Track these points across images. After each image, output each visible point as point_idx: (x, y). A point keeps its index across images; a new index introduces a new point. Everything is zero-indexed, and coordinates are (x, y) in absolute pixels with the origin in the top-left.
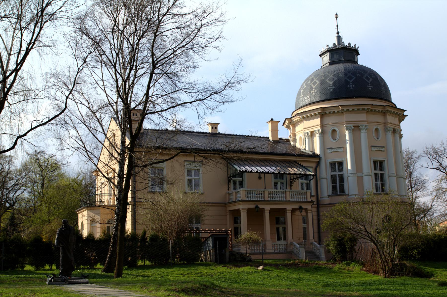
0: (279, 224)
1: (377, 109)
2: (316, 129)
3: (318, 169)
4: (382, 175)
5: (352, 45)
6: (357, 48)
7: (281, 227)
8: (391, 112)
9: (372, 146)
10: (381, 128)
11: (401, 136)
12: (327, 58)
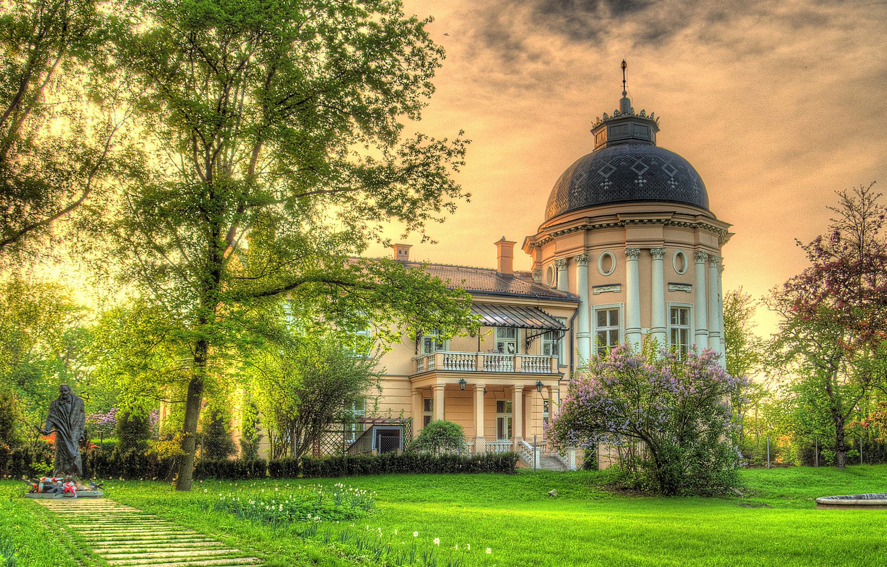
0: (502, 412)
1: (604, 223)
2: (577, 254)
3: (575, 321)
4: (684, 332)
5: (648, 114)
6: (655, 118)
7: (505, 416)
8: (706, 227)
9: (669, 284)
10: (688, 254)
11: (721, 269)
12: (604, 134)
